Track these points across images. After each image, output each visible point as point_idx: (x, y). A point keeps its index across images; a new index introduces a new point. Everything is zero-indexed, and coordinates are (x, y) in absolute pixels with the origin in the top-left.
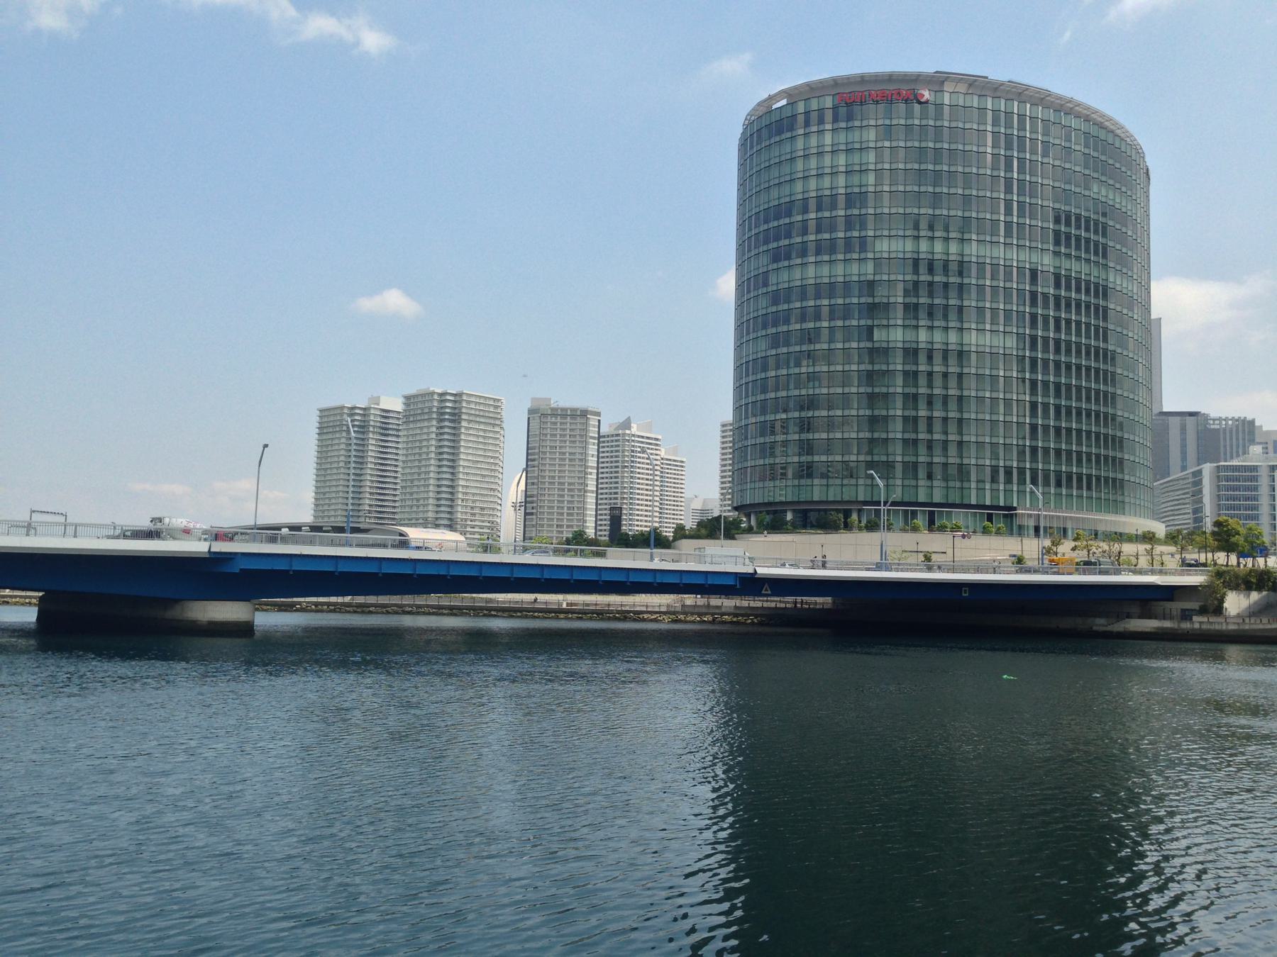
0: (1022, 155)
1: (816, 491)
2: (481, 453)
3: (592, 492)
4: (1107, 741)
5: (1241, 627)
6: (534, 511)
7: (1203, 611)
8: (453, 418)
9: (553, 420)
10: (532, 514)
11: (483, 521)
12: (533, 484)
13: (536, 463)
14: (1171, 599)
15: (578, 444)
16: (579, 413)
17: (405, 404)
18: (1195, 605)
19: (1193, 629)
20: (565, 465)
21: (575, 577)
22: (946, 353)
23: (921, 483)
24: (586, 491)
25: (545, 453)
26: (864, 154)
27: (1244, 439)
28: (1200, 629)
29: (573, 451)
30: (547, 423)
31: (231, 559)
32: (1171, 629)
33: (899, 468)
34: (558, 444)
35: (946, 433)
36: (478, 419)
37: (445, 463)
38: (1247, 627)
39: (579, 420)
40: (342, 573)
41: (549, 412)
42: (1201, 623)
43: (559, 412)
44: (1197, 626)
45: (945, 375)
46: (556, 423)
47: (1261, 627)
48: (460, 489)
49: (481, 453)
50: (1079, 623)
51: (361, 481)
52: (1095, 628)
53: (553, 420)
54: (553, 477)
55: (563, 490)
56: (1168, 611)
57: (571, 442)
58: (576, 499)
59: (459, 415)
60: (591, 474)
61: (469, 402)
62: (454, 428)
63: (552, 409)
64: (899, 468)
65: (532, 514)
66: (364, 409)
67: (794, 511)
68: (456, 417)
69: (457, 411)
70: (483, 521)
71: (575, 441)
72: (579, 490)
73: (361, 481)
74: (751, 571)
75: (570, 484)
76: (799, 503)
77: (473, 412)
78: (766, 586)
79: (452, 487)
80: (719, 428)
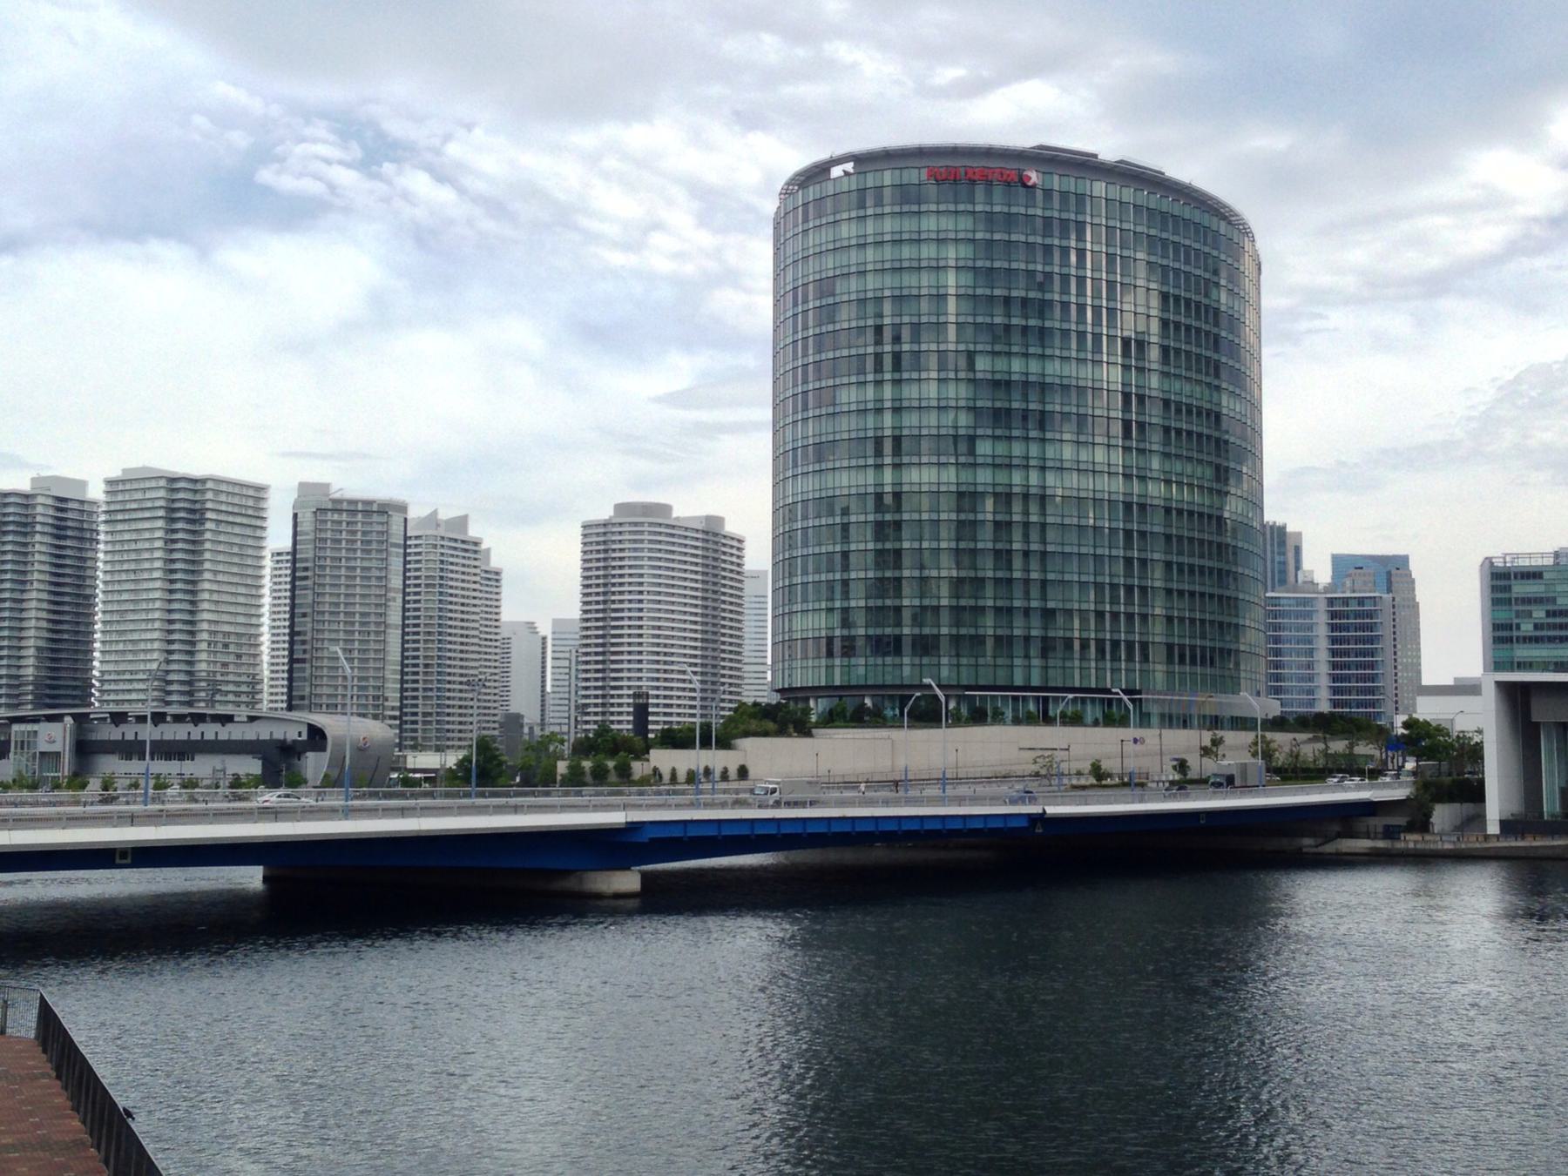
0: (1111, 278)
1: (907, 671)
2: (235, 570)
3: (396, 627)
4: (1151, 968)
5: (1458, 846)
6: (307, 656)
7: (1411, 828)
8: (191, 516)
9: (336, 517)
10: (303, 661)
11: (240, 675)
12: (304, 615)
13: (309, 583)
14: (1373, 814)
15: (374, 555)
16: (375, 508)
17: (107, 492)
18: (1401, 821)
19: (1408, 849)
20: (355, 586)
21: (926, 827)
22: (1026, 497)
23: (1018, 662)
24: (386, 626)
25: (323, 567)
26: (941, 273)
27: (1273, 552)
28: (1415, 849)
29: (366, 564)
30: (326, 521)
31: (636, 829)
32: (1387, 849)
33: (990, 644)
34: (344, 554)
35: (1028, 599)
36: (231, 519)
37: (179, 586)
38: (1463, 846)
39: (375, 518)
40: (725, 837)
41: (330, 507)
42: (1416, 842)
43: (345, 506)
44: (1411, 845)
45: (1026, 525)
46: (340, 522)
47: (1478, 845)
48: (205, 626)
49: (235, 570)
50: (1285, 843)
51: (23, 610)
52: (1305, 850)
53: (336, 517)
54: (337, 605)
55: (353, 623)
56: (1372, 829)
57: (363, 551)
58: (372, 637)
59: (203, 511)
60: (394, 599)
61: (217, 492)
62: (194, 532)
63: (335, 501)
64: (990, 644)
65: (303, 661)
66: (27, 496)
67: (873, 696)
68: (196, 515)
69: (198, 506)
70: (240, 675)
71: (371, 550)
72: (378, 624)
73: (23, 610)
74: (1040, 811)
75: (362, 614)
76: (883, 687)
77: (223, 508)
78: (1039, 825)
79: (192, 623)
80: (579, 531)
